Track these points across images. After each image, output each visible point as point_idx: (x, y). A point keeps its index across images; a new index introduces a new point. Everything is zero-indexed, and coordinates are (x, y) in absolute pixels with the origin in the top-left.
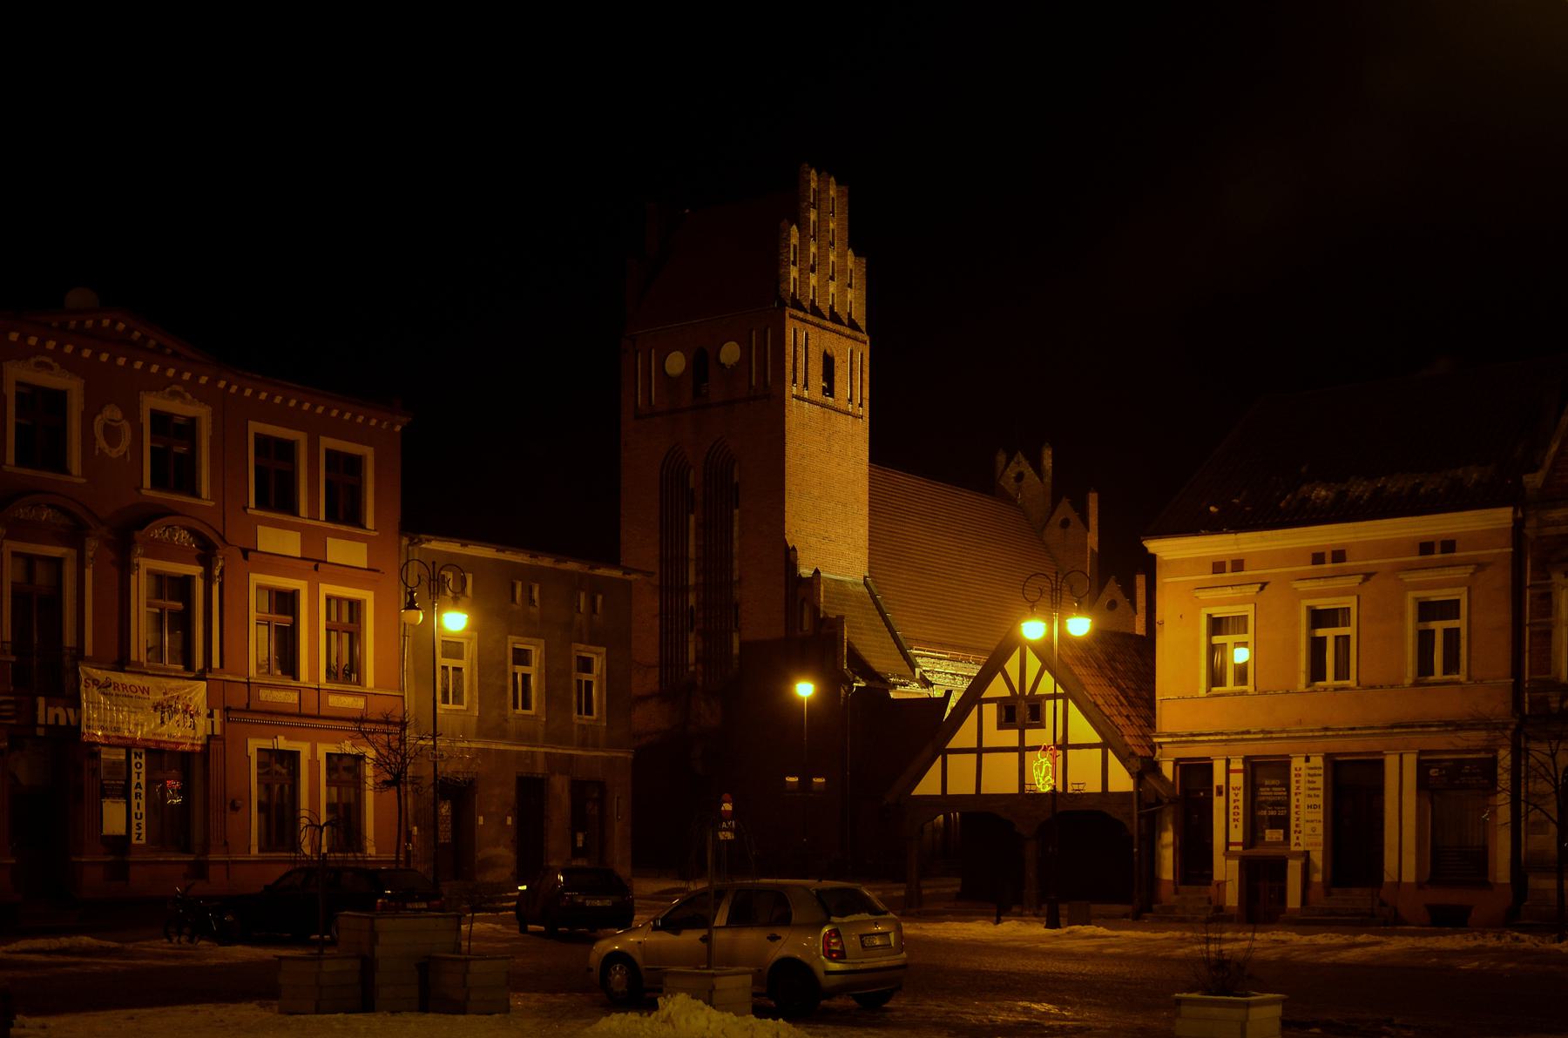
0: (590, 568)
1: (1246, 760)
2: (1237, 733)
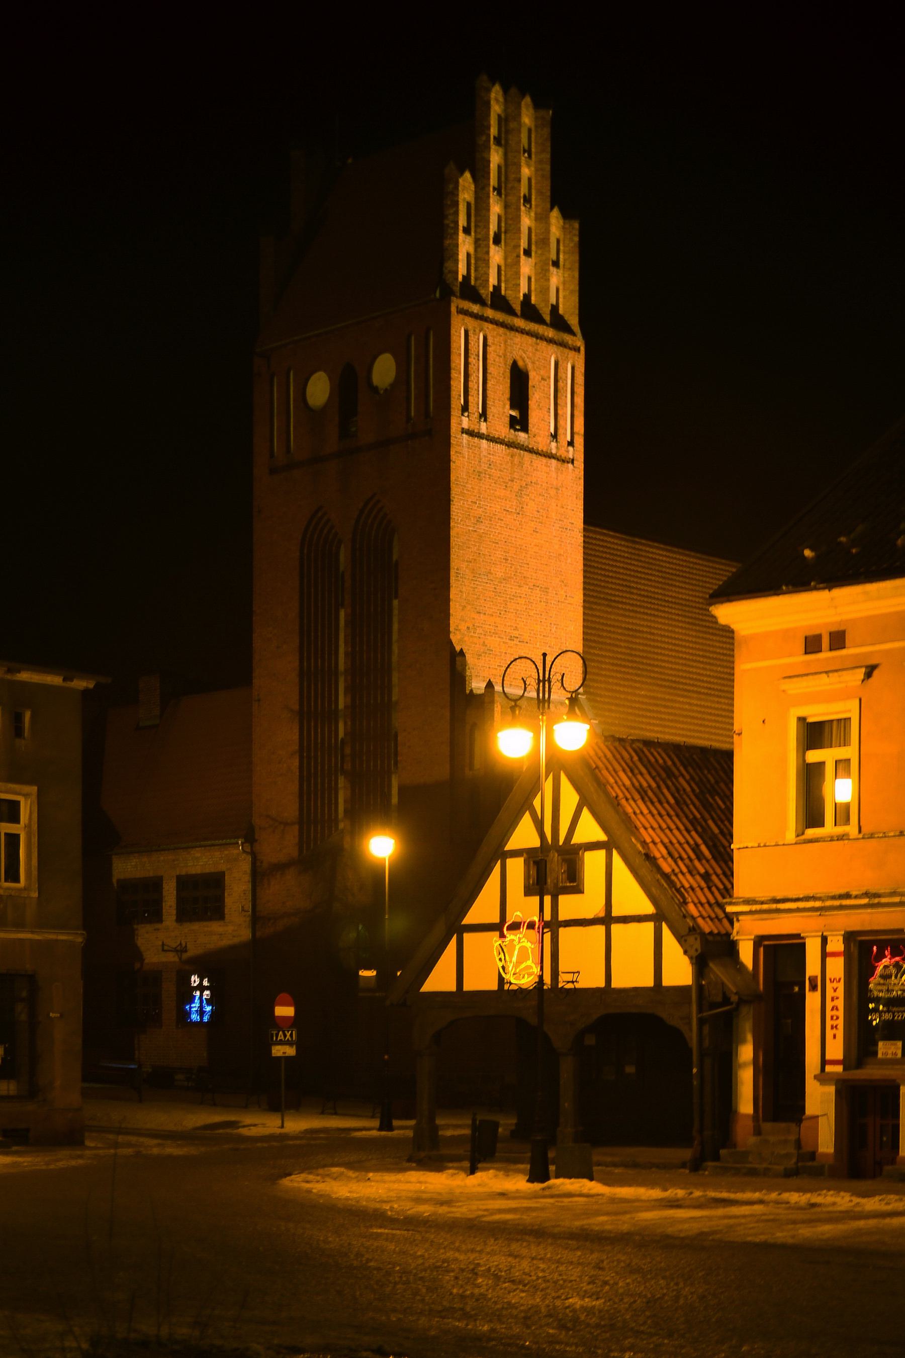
0: (9, 671)
1: (849, 937)
2: (833, 898)
